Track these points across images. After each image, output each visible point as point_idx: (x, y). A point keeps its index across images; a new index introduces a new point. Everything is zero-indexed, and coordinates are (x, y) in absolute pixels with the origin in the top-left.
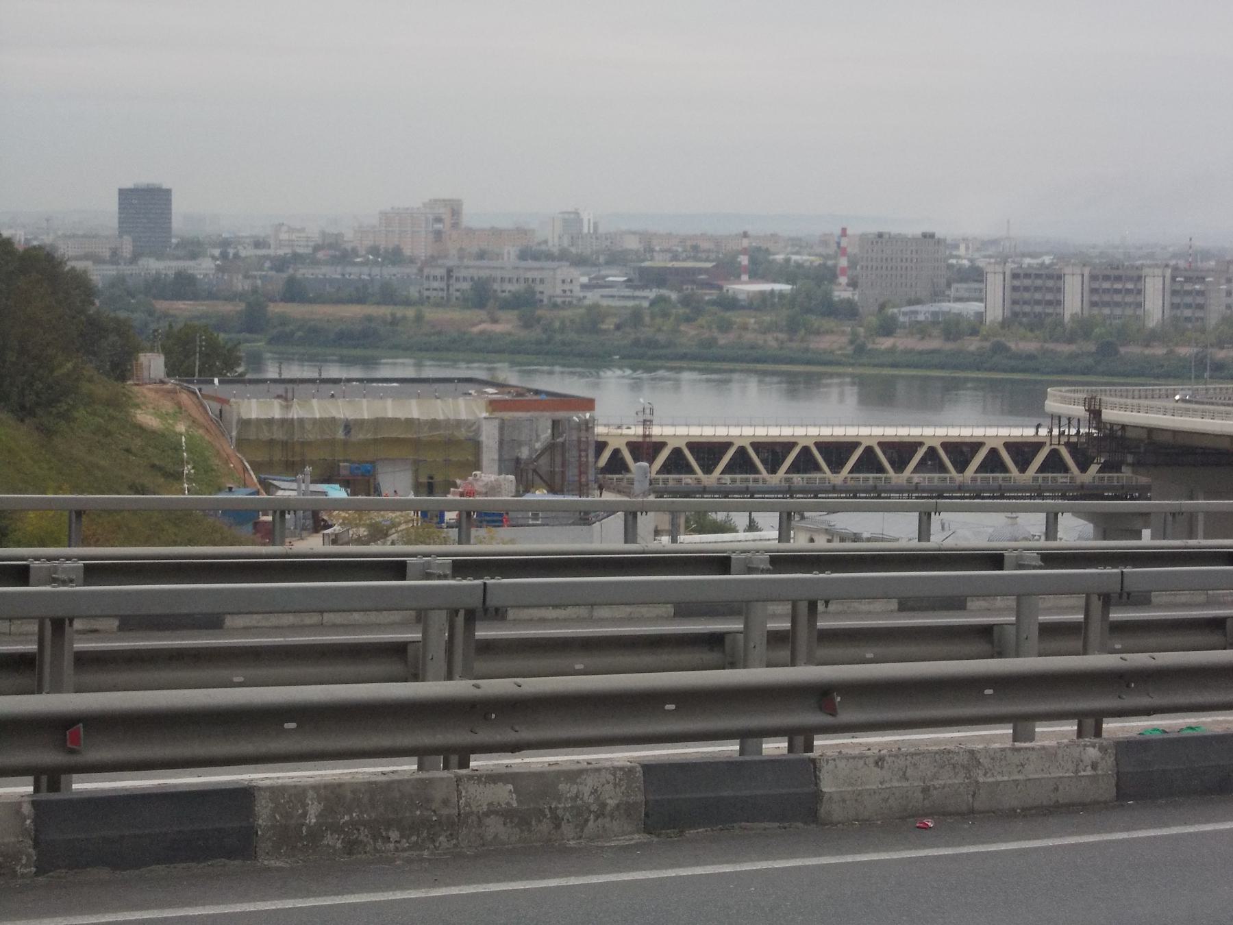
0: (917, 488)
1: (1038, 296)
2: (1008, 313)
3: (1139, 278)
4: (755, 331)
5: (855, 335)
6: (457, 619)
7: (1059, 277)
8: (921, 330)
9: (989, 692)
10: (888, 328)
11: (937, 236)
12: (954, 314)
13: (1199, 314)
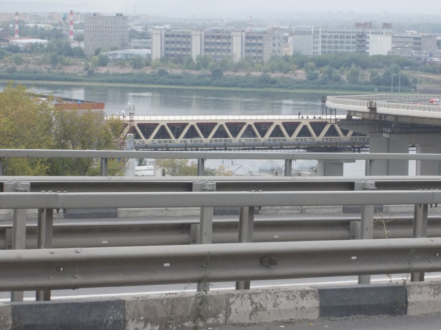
0: (244, 145)
1: (178, 46)
2: (163, 55)
3: (230, 37)
4: (34, 63)
5: (86, 65)
6: (43, 214)
7: (189, 37)
8: (121, 63)
9: (354, 258)
10: (104, 62)
11: (124, 15)
12: (136, 55)
13: (260, 55)
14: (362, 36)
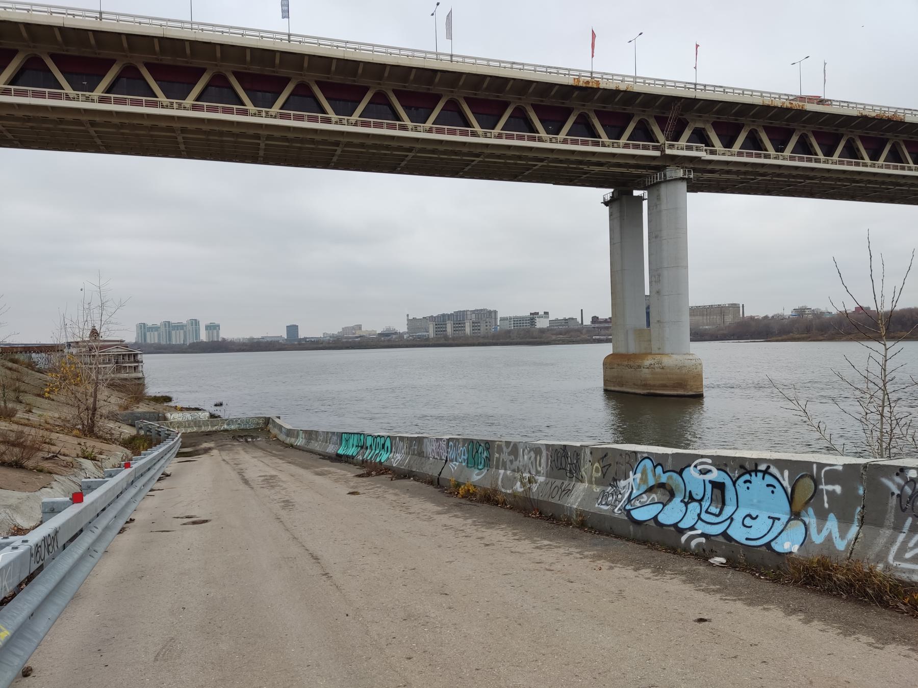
1: (441, 329)
13: (479, 331)
14: (532, 319)
